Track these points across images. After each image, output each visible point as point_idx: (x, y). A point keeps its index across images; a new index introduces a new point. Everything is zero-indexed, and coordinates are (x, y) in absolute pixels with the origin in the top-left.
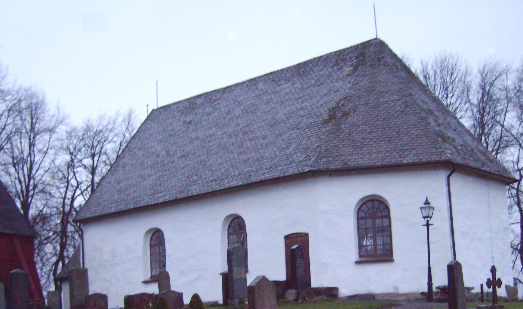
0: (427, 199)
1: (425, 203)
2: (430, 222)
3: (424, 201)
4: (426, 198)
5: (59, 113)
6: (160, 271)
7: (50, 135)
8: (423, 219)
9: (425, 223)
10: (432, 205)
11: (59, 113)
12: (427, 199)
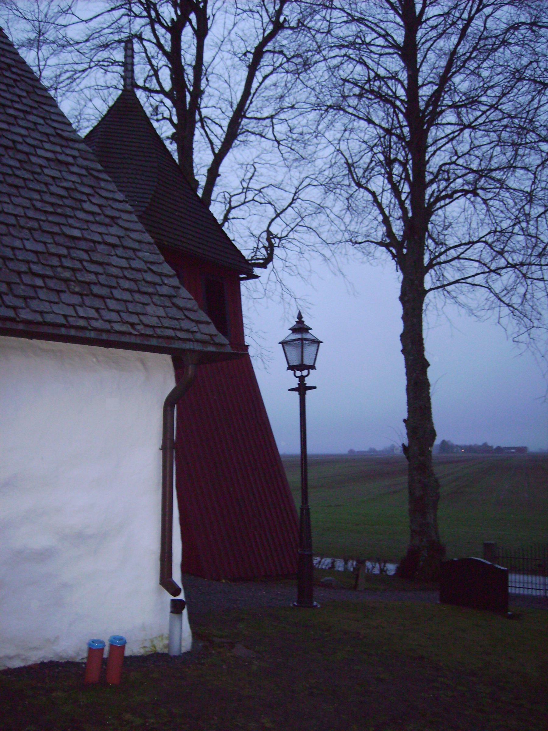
0: (300, 316)
1: (294, 330)
2: (309, 382)
3: (293, 322)
4: (296, 315)
5: (471, 133)
6: (182, 287)
7: (281, 184)
8: (291, 372)
9: (295, 383)
10: (315, 333)
11: (471, 133)
12: (300, 316)
